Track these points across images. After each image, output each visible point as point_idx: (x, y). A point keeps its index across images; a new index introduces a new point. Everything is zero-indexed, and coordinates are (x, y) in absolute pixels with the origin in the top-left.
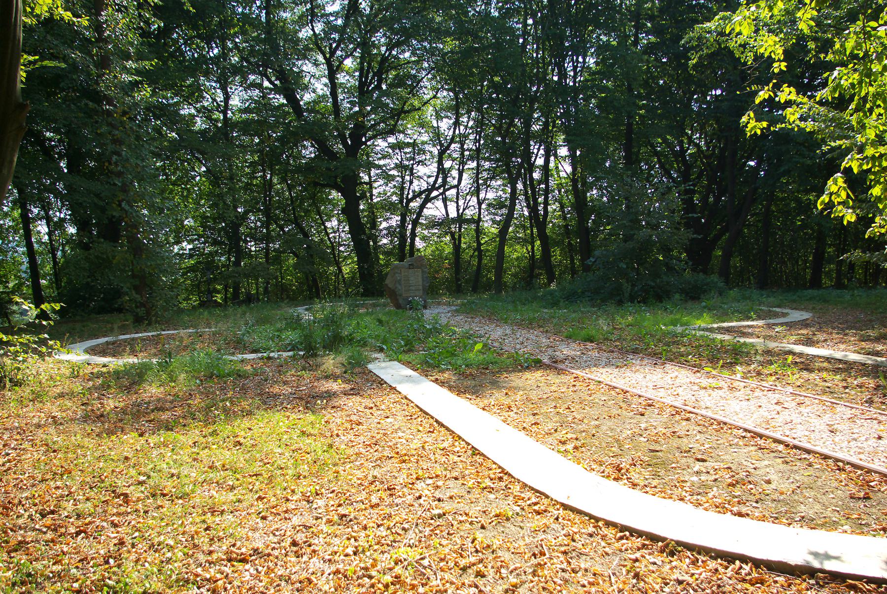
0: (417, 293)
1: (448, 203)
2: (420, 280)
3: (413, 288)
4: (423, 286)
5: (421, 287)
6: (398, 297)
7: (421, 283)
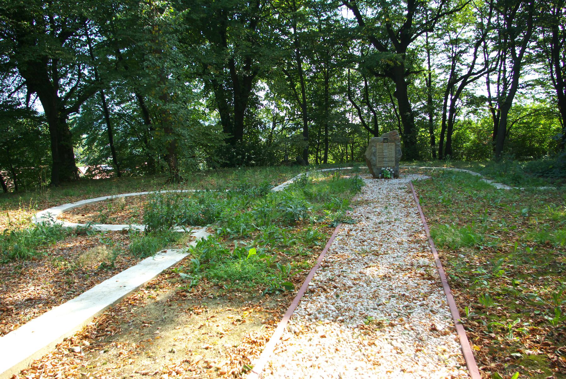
0: (390, 164)
1: (491, 85)
2: (393, 152)
3: (387, 160)
4: (396, 158)
5: (394, 159)
6: (373, 167)
7: (394, 155)
